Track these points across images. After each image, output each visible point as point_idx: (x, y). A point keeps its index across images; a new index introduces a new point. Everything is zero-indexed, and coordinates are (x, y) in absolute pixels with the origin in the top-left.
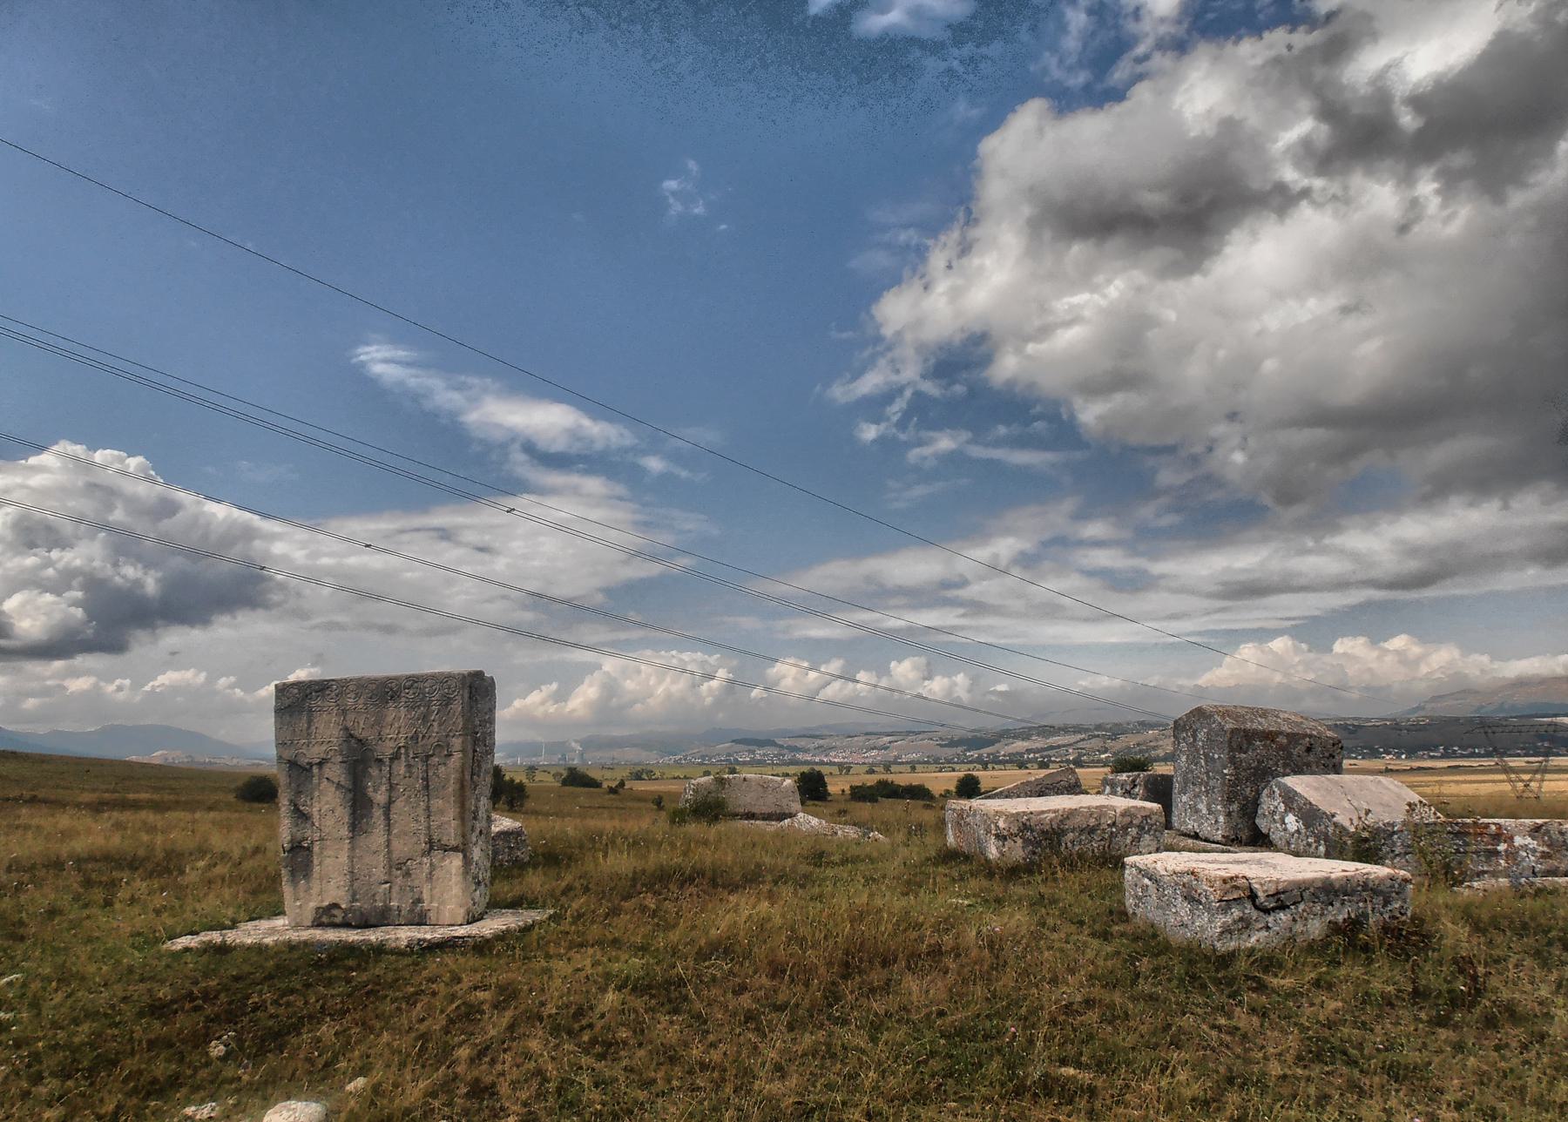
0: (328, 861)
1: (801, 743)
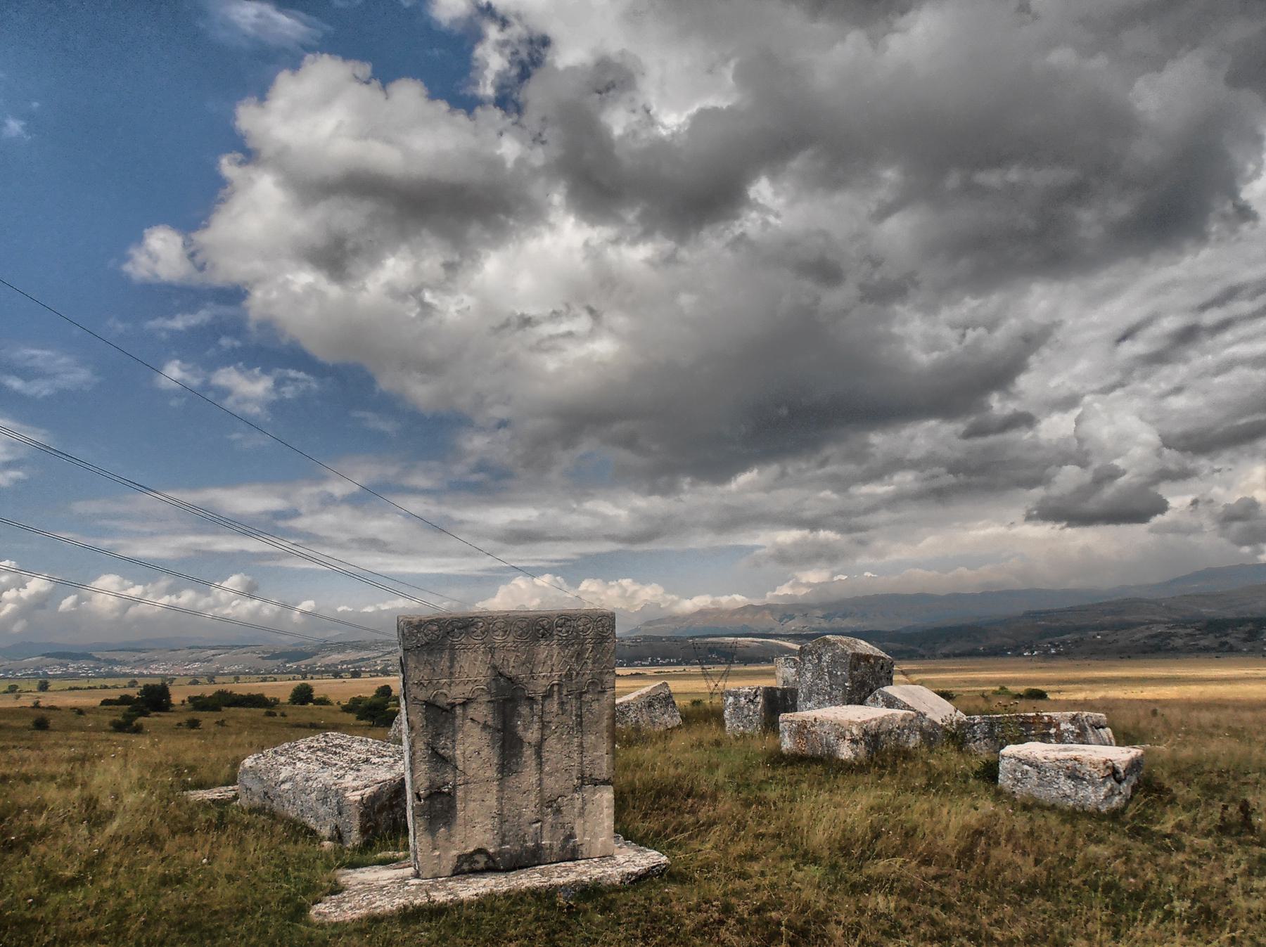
0: (472, 805)
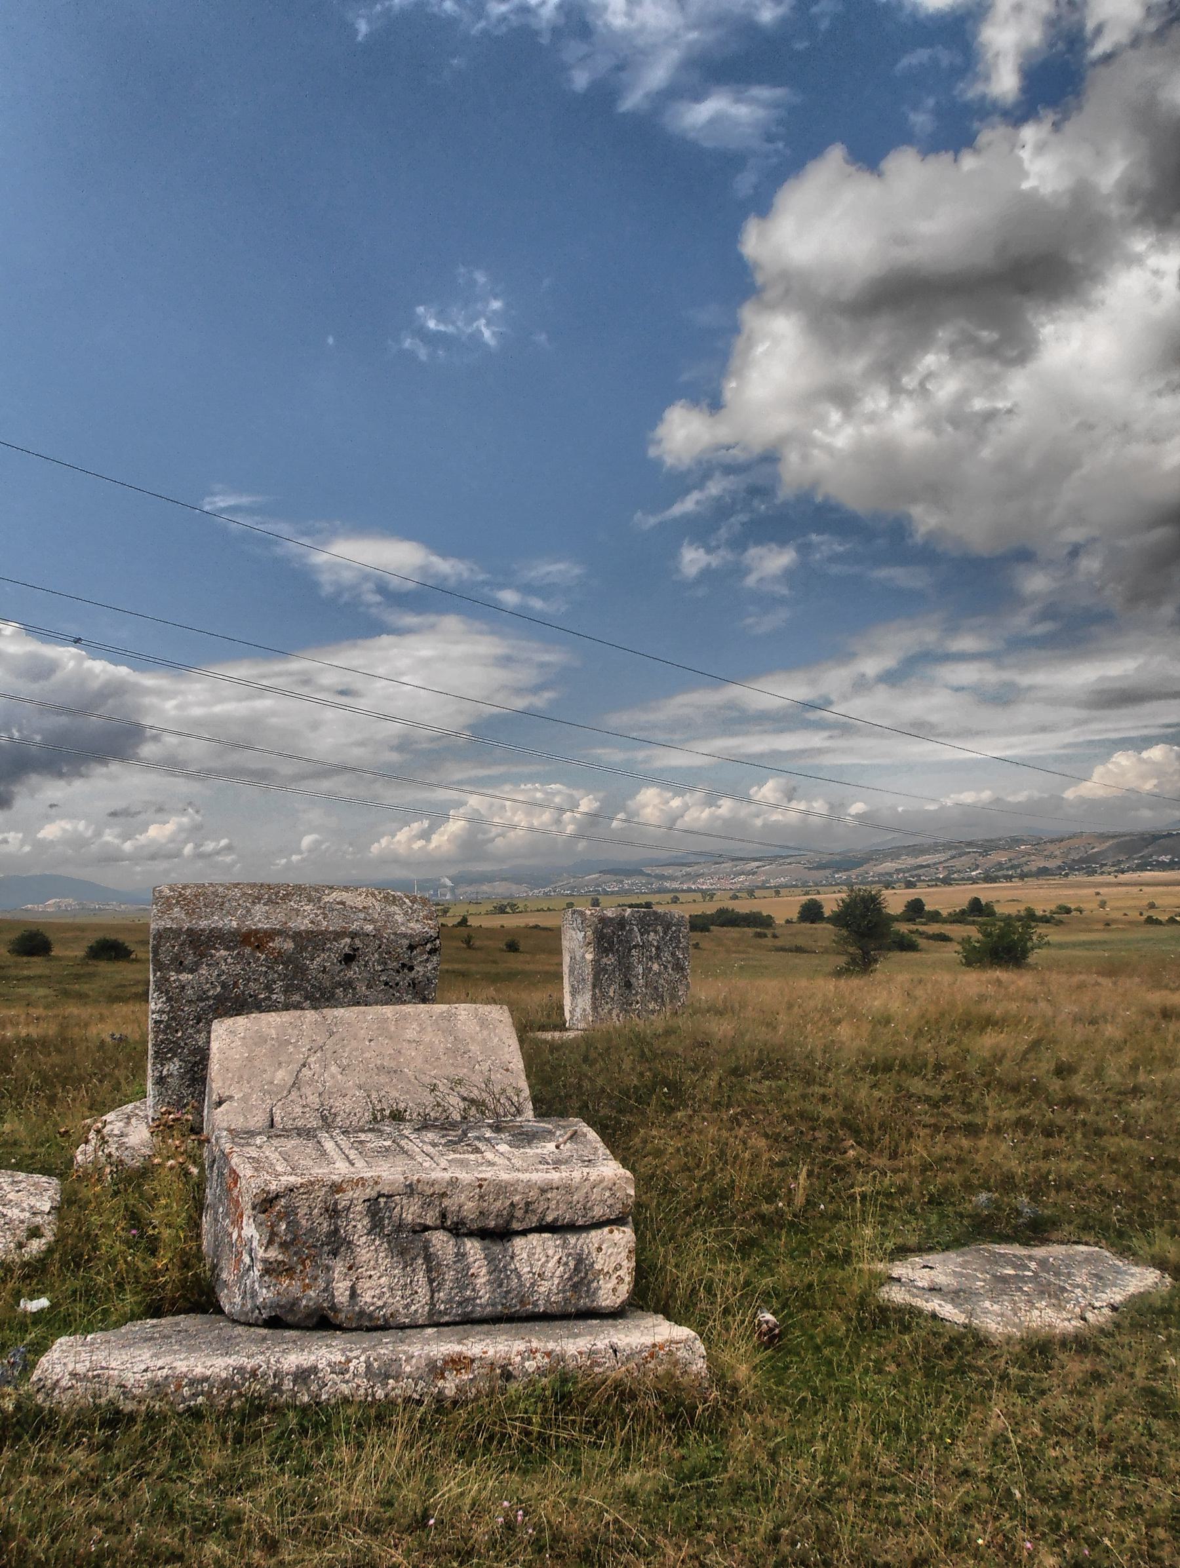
1: (668, 871)
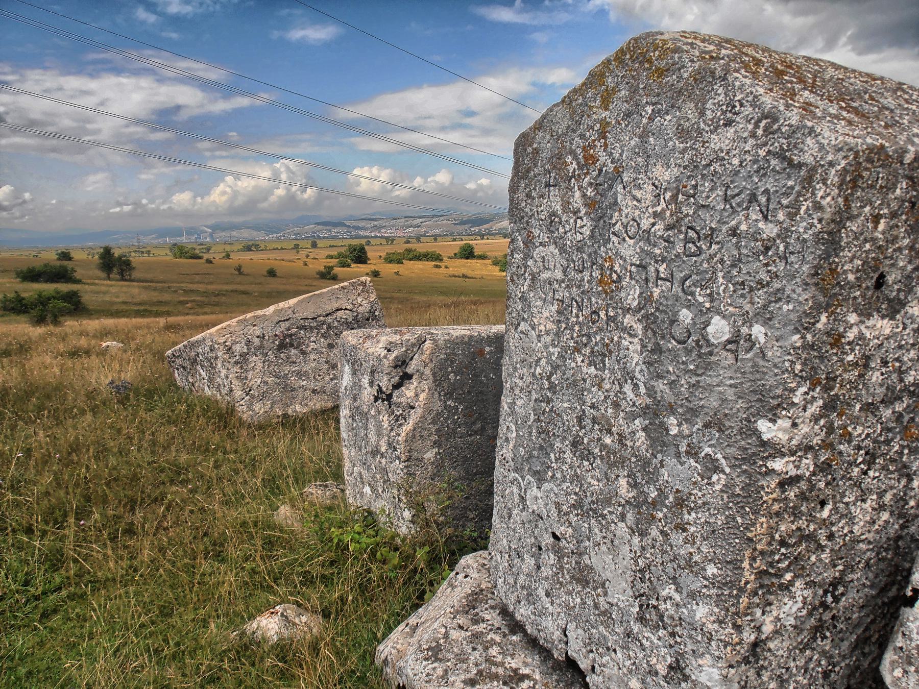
1: (362, 224)
